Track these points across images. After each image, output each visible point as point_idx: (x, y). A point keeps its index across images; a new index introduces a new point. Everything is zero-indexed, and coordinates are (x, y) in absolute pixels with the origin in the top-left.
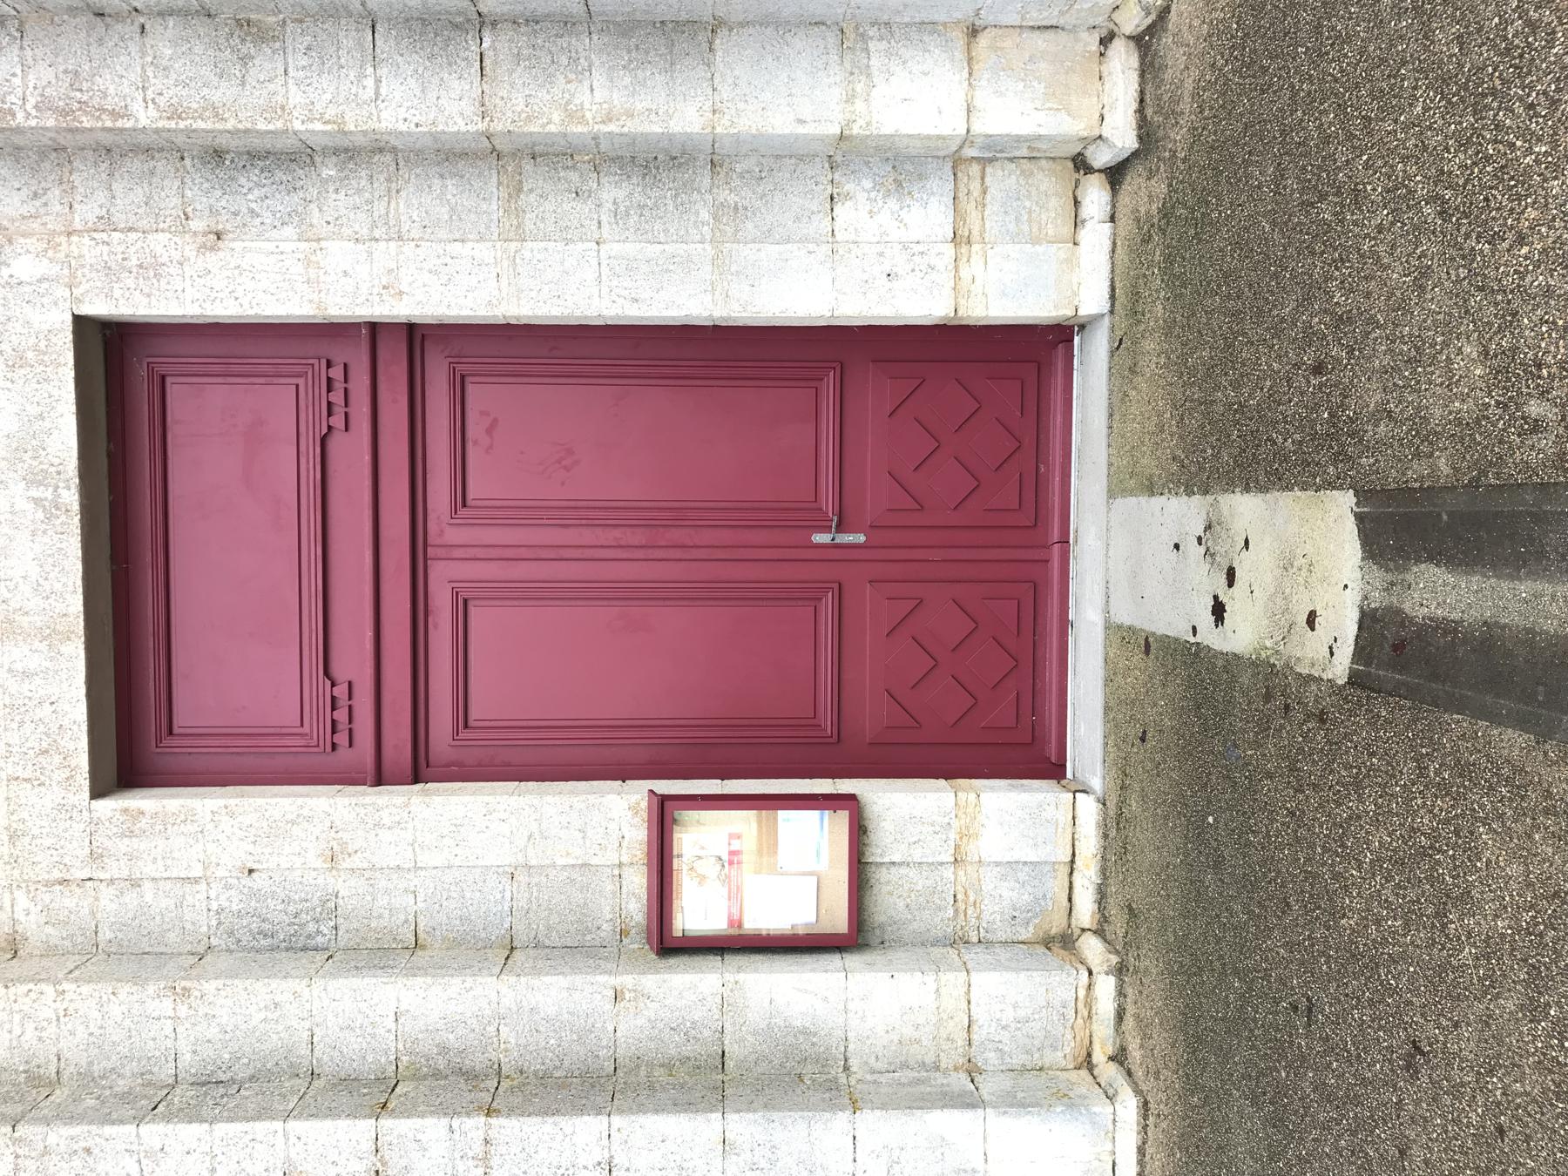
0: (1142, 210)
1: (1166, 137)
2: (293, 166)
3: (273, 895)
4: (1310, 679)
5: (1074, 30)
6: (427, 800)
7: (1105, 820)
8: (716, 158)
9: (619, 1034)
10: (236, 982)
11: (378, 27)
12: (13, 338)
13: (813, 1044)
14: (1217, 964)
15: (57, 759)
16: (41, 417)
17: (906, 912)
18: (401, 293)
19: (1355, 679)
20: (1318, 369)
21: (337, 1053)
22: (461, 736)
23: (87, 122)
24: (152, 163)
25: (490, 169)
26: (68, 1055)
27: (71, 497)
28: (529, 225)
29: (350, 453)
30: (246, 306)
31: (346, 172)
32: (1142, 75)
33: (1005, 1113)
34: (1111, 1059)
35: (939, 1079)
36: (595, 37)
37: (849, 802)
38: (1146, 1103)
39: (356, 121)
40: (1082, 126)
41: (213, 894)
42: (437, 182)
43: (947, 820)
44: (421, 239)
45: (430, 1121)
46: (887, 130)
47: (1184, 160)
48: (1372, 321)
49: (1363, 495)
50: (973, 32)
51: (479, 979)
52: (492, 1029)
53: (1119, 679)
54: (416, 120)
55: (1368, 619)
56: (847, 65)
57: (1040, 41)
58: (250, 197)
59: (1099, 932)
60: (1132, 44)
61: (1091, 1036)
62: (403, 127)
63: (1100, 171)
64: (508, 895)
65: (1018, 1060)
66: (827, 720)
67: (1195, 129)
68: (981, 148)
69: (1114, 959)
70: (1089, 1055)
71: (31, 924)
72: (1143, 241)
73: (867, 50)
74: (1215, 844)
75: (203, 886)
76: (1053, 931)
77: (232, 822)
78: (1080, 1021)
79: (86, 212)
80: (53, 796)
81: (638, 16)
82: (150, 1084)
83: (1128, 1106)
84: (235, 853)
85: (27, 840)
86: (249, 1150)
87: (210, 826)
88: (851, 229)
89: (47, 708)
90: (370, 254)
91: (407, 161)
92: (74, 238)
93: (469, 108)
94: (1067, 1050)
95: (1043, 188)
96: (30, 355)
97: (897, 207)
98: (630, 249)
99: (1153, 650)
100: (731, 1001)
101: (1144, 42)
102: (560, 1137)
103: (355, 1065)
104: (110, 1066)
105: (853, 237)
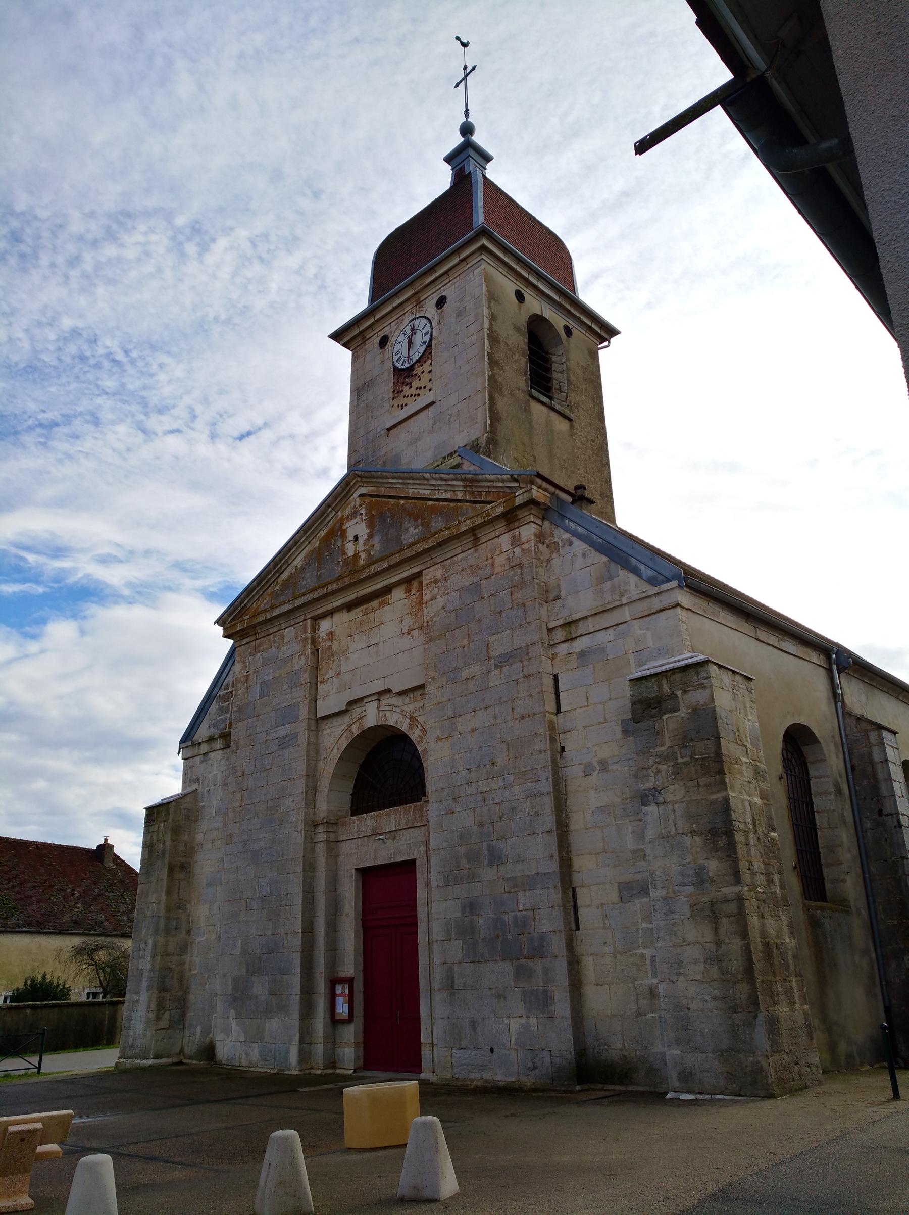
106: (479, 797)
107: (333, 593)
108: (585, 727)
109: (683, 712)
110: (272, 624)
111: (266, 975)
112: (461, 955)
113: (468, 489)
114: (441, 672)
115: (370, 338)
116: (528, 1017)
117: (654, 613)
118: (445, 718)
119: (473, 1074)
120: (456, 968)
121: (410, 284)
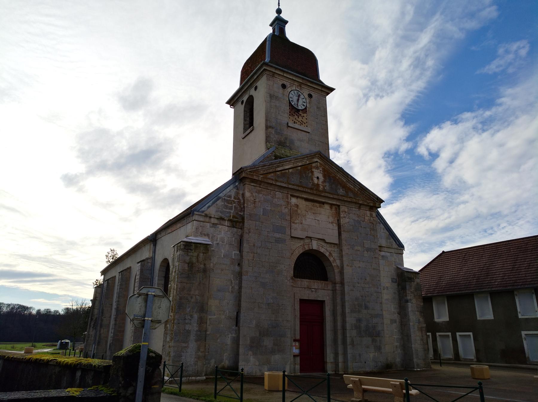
27: (316, 299)
107: (305, 192)
108: (383, 276)
109: (415, 283)
110: (271, 186)
113: (360, 190)
115: (276, 78)
116: (375, 353)
117: (399, 254)
121: (303, 79)
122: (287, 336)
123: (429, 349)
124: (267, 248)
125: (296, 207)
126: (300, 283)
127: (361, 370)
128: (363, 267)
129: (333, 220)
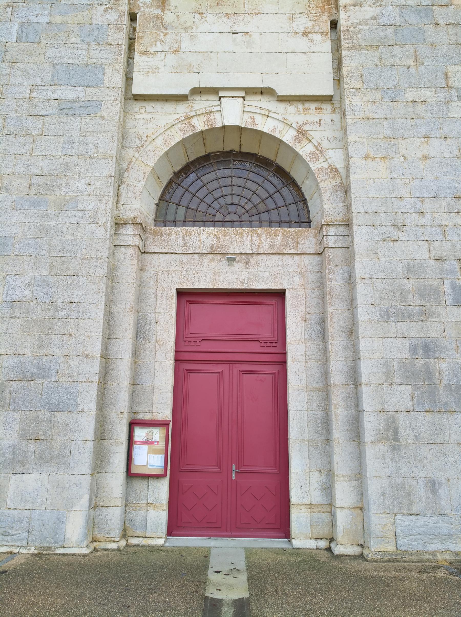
0: (319, 556)
1: (336, 561)
2: (322, 338)
3: (151, 328)
4: (205, 590)
5: (364, 537)
6: (172, 365)
7: (157, 547)
8: (329, 440)
9: (112, 413)
10: (133, 322)
11: (353, 361)
12: (281, 276)
13: (105, 464)
14: (130, 571)
15: (186, 281)
16: (263, 281)
17: (135, 489)
18: (293, 362)
19: (206, 598)
20: (276, 591)
21: (113, 344)
22: (186, 371)
23: (328, 297)
24: (321, 307)
25: (324, 384)
26: (119, 285)
27: (245, 287)
28: (311, 393)
29: (255, 347)
30: (289, 326)
31: (321, 350)
32: (353, 556)
33: (87, 516)
34: (95, 548)
35: (94, 498)
36: (354, 412)
37: (165, 475)
38: (87, 556)
39: (332, 355)
40: (340, 539)
41: (152, 314)
42: (320, 371)
43: (159, 501)
44: (306, 367)
45: (98, 369)
46: (336, 486)
47: (329, 565)
48: (287, 600)
49: (248, 599)
50: (361, 509)
51: (129, 379)
52: (116, 381)
53: (196, 550)
54: (333, 369)
55: (220, 601)
56: (351, 475)
57: (360, 527)
58: (314, 328)
59: (127, 545)
60: (361, 553)
61: (101, 542)
62: (331, 366)
63: (330, 545)
64: (147, 384)
65: (96, 521)
66: (185, 468)
67: (337, 567)
68: (334, 511)
69: (122, 548)
70: (96, 541)
71: (147, 274)
72: (311, 556)
73: (355, 480)
74: (160, 571)
75: (154, 312)
76: (127, 532)
77: (169, 319)
78: (105, 538)
79: (309, 292)
80: (177, 279)
81: (360, 423)
82: (110, 302)
83: (85, 551)
84: (161, 319)
85: (168, 274)
86: (96, 327)
87: (168, 314)
88: (313, 476)
89: (197, 280)
90: (302, 355)
91: (325, 364)
92: (303, 290)
93: (336, 382)
94: (98, 535)
95: (325, 529)
96: (277, 279)
97: (319, 488)
98: (306, 418)
99: (205, 558)
100: (118, 442)
101: (361, 556)
102: (91, 399)
103: (110, 348)
104: (115, 293)
105: (311, 476)
106: (436, 230)
111: (14, 410)
112: (411, 403)
114: (372, 86)
118: (379, 136)
119: (432, 545)
120: (402, 419)
122: (80, 408)
123: (62, 554)
124: (24, 133)
125: (159, 7)
126: (180, 239)
127: (441, 547)
128: (447, 155)
129: (309, 24)
